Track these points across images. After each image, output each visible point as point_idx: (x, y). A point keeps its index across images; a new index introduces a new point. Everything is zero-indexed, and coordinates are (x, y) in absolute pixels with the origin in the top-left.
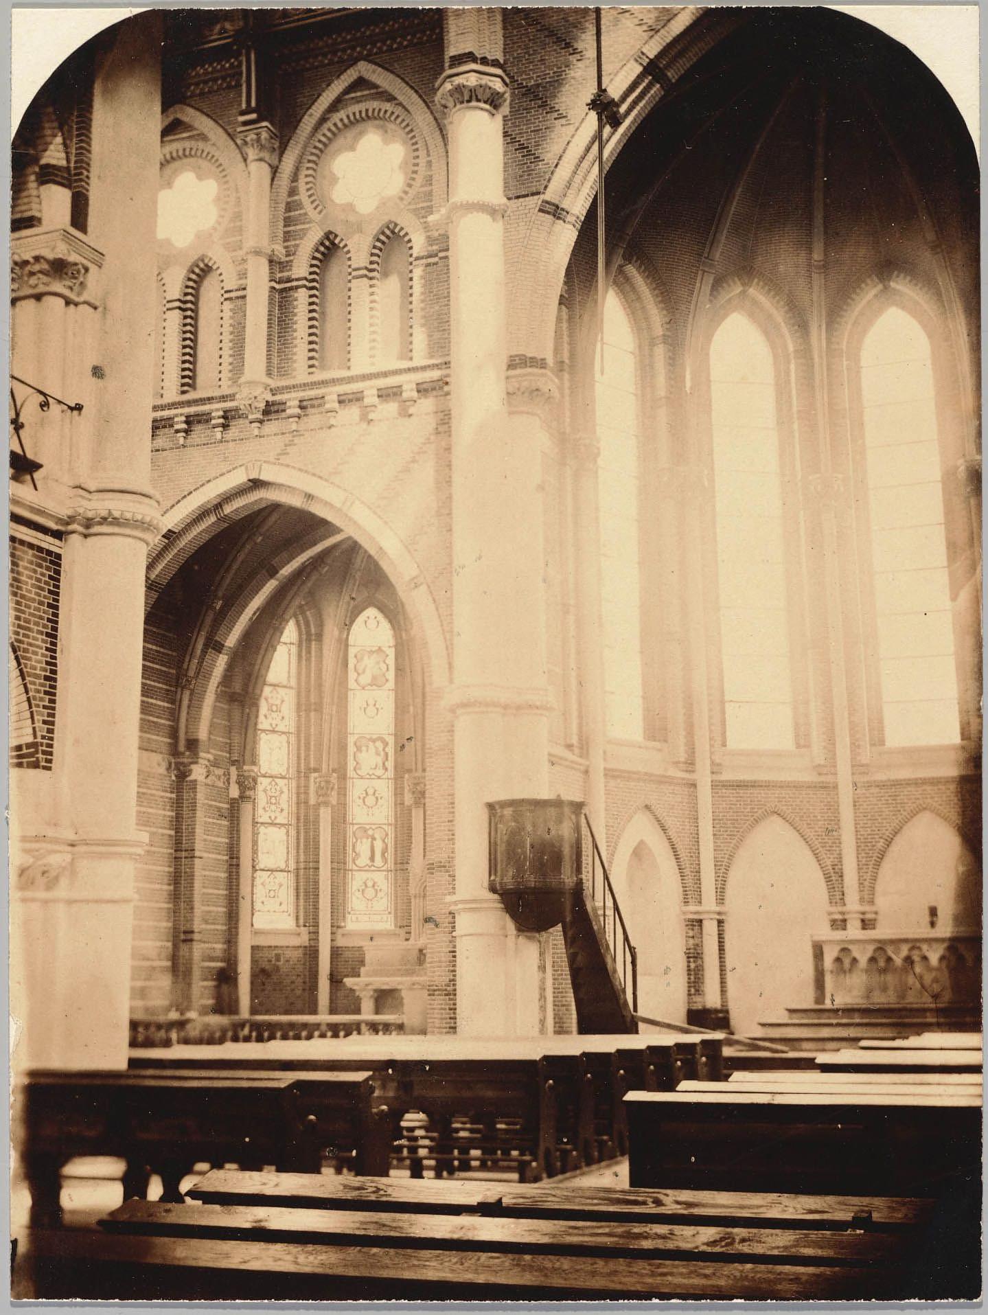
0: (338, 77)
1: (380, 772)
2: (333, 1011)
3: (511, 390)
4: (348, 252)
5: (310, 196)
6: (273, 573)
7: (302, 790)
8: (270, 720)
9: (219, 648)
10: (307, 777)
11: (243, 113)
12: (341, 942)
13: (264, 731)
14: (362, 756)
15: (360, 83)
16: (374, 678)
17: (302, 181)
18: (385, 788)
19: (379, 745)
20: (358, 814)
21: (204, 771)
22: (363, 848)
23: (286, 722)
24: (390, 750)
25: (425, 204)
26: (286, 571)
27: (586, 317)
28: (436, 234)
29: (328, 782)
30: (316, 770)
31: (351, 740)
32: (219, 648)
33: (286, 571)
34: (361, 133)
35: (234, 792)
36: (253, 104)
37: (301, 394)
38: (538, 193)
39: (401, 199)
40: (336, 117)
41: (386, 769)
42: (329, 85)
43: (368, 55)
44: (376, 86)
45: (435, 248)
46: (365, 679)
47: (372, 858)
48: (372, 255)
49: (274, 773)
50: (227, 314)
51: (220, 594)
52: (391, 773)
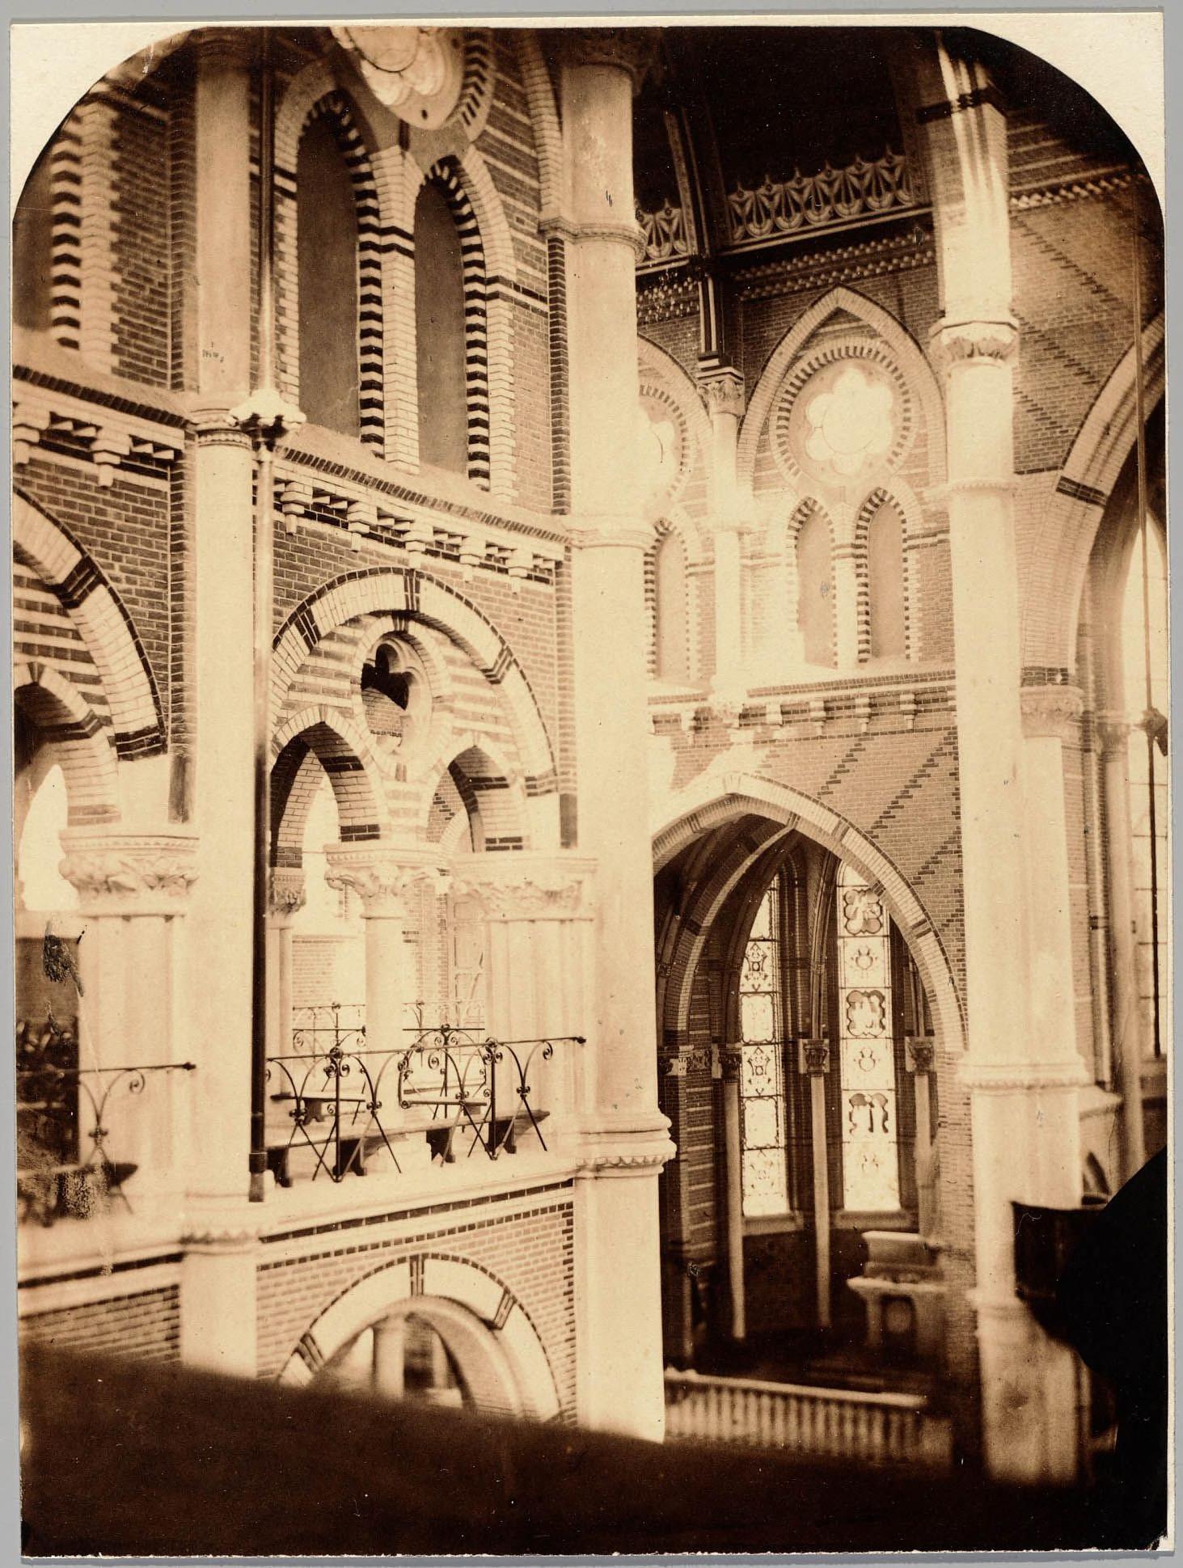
1: (877, 1030)
3: (1027, 709)
4: (826, 515)
5: (783, 453)
6: (752, 848)
8: (751, 982)
10: (795, 1044)
11: (702, 359)
12: (841, 1224)
13: (745, 994)
14: (856, 1014)
15: (838, 314)
16: (866, 922)
17: (773, 432)
18: (884, 1051)
19: (875, 1000)
21: (685, 1065)
23: (769, 979)
25: (920, 470)
27: (1113, 560)
29: (819, 1050)
31: (843, 995)
32: (696, 929)
34: (841, 373)
35: (717, 1072)
36: (714, 348)
37: (782, 699)
38: (1056, 468)
39: (891, 462)
40: (810, 356)
41: (883, 1027)
42: (800, 317)
43: (847, 281)
45: (933, 525)
46: (856, 925)
48: (858, 527)
49: (758, 1039)
50: (693, 591)
51: (695, 875)
52: (889, 1032)
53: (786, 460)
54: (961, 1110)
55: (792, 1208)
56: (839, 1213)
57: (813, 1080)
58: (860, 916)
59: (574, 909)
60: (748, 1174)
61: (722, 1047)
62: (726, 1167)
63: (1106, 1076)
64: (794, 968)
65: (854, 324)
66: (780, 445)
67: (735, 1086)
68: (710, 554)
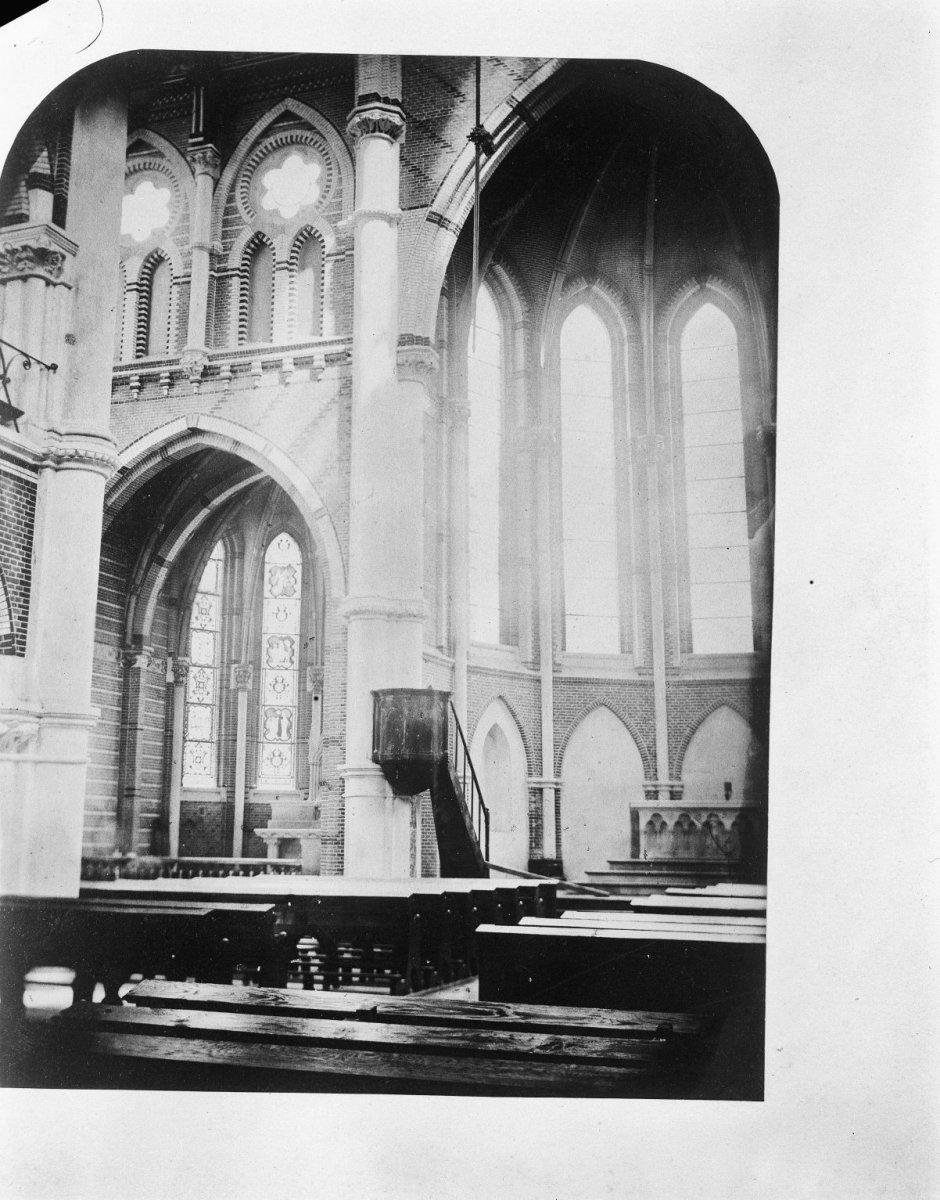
0: (270, 110)
1: (287, 664)
2: (244, 855)
6: (206, 503)
7: (225, 677)
9: (161, 562)
10: (229, 667)
12: (253, 800)
13: (195, 629)
15: (287, 115)
17: (238, 191)
18: (291, 677)
19: (288, 643)
20: (269, 697)
22: (273, 725)
24: (296, 647)
26: (217, 501)
28: (343, 236)
30: (236, 662)
31: (265, 638)
32: (161, 562)
33: (217, 501)
35: (170, 678)
36: (201, 129)
37: (232, 361)
38: (426, 206)
39: (317, 208)
44: (300, 118)
46: (277, 590)
47: (279, 734)
50: (175, 296)
52: (296, 665)
53: (246, 208)
54: (340, 638)
55: (218, 786)
56: (252, 791)
57: (240, 694)
58: (280, 584)
59: (58, 277)
60: (189, 759)
61: (174, 659)
62: (171, 747)
63: (444, 643)
64: (231, 615)
65: (297, 122)
66: (243, 198)
67: (182, 689)
68: (188, 270)
